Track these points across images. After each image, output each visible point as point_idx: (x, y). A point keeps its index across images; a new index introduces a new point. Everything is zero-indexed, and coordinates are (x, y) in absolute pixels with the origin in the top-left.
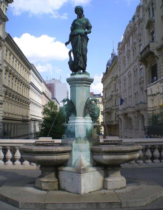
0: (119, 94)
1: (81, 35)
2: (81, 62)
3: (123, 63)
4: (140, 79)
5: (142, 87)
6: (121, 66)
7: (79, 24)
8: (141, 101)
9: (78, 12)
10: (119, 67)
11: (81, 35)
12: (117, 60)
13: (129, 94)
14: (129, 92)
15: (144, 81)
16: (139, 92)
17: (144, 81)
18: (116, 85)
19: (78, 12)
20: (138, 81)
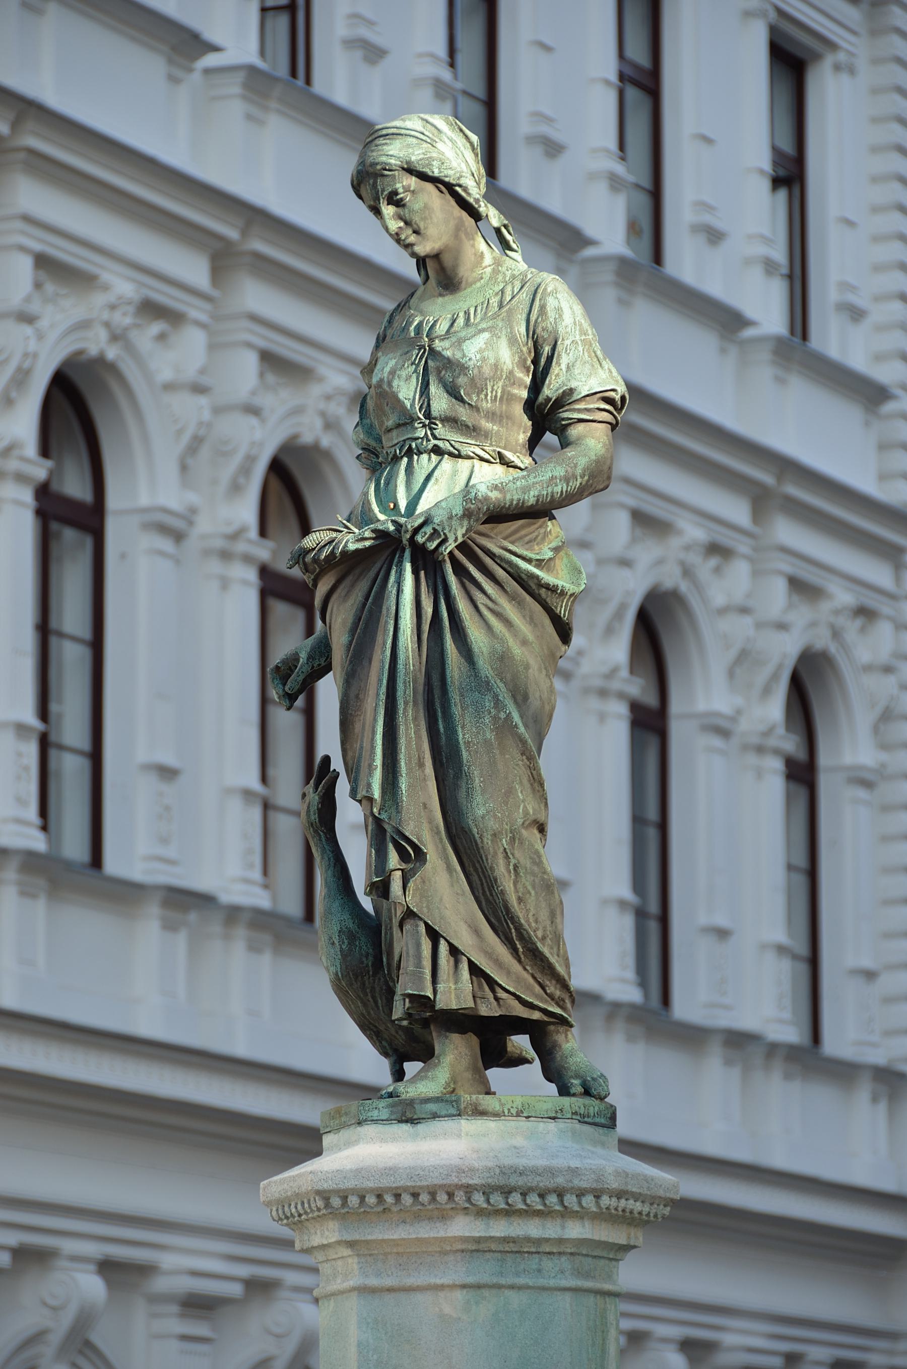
1: (427, 562)
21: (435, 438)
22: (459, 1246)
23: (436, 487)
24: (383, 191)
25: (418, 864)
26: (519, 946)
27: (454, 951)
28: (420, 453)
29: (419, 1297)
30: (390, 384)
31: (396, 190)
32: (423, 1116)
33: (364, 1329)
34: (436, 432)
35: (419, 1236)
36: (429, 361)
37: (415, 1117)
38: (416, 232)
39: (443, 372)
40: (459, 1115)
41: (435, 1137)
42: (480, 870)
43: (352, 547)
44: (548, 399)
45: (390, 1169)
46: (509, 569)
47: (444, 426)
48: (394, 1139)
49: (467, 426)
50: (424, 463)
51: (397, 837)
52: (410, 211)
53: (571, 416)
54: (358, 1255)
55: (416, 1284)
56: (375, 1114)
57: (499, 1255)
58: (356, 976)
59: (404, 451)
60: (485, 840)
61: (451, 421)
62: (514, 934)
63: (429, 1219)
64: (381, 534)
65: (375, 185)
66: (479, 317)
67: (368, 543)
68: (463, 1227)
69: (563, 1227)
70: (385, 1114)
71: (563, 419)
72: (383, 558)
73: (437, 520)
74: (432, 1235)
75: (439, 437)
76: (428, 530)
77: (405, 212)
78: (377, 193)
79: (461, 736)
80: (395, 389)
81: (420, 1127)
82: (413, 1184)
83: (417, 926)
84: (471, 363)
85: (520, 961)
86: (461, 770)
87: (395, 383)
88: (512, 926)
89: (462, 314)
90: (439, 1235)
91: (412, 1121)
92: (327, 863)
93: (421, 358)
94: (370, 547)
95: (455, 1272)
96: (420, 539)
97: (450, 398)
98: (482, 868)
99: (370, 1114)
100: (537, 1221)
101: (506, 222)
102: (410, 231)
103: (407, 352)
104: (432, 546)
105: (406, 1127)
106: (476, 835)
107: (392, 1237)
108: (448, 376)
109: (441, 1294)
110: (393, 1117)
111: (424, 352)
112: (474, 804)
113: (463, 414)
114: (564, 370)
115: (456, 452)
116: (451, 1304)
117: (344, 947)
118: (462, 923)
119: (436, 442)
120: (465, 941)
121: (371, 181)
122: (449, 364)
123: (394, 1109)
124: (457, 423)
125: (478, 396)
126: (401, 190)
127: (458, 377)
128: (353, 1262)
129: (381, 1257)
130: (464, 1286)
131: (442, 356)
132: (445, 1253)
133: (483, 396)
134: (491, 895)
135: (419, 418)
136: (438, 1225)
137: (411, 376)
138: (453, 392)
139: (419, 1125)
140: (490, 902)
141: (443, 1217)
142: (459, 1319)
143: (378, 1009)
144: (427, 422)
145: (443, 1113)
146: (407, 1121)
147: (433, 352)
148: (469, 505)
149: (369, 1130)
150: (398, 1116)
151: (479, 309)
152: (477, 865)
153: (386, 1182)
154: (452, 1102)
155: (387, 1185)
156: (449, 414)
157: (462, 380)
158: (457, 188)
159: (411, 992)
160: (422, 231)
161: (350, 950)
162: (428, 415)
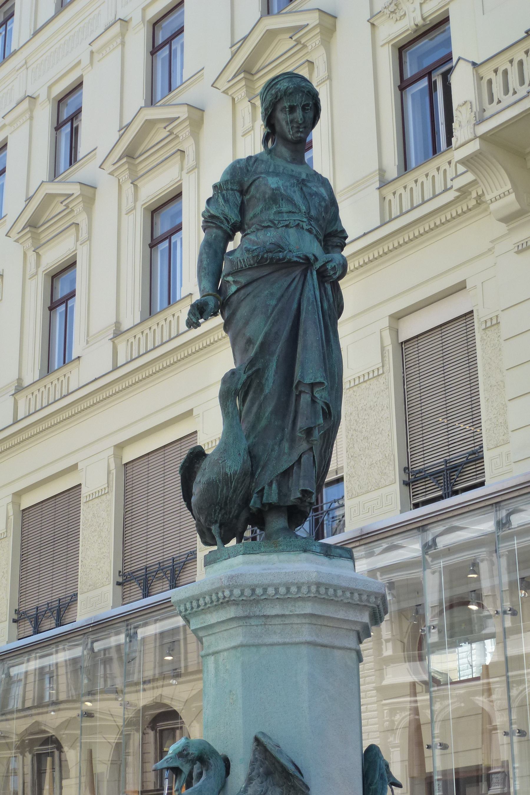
51: (325, 408)
74: (356, 620)
110: (322, 552)
134: (325, 452)
139: (333, 560)
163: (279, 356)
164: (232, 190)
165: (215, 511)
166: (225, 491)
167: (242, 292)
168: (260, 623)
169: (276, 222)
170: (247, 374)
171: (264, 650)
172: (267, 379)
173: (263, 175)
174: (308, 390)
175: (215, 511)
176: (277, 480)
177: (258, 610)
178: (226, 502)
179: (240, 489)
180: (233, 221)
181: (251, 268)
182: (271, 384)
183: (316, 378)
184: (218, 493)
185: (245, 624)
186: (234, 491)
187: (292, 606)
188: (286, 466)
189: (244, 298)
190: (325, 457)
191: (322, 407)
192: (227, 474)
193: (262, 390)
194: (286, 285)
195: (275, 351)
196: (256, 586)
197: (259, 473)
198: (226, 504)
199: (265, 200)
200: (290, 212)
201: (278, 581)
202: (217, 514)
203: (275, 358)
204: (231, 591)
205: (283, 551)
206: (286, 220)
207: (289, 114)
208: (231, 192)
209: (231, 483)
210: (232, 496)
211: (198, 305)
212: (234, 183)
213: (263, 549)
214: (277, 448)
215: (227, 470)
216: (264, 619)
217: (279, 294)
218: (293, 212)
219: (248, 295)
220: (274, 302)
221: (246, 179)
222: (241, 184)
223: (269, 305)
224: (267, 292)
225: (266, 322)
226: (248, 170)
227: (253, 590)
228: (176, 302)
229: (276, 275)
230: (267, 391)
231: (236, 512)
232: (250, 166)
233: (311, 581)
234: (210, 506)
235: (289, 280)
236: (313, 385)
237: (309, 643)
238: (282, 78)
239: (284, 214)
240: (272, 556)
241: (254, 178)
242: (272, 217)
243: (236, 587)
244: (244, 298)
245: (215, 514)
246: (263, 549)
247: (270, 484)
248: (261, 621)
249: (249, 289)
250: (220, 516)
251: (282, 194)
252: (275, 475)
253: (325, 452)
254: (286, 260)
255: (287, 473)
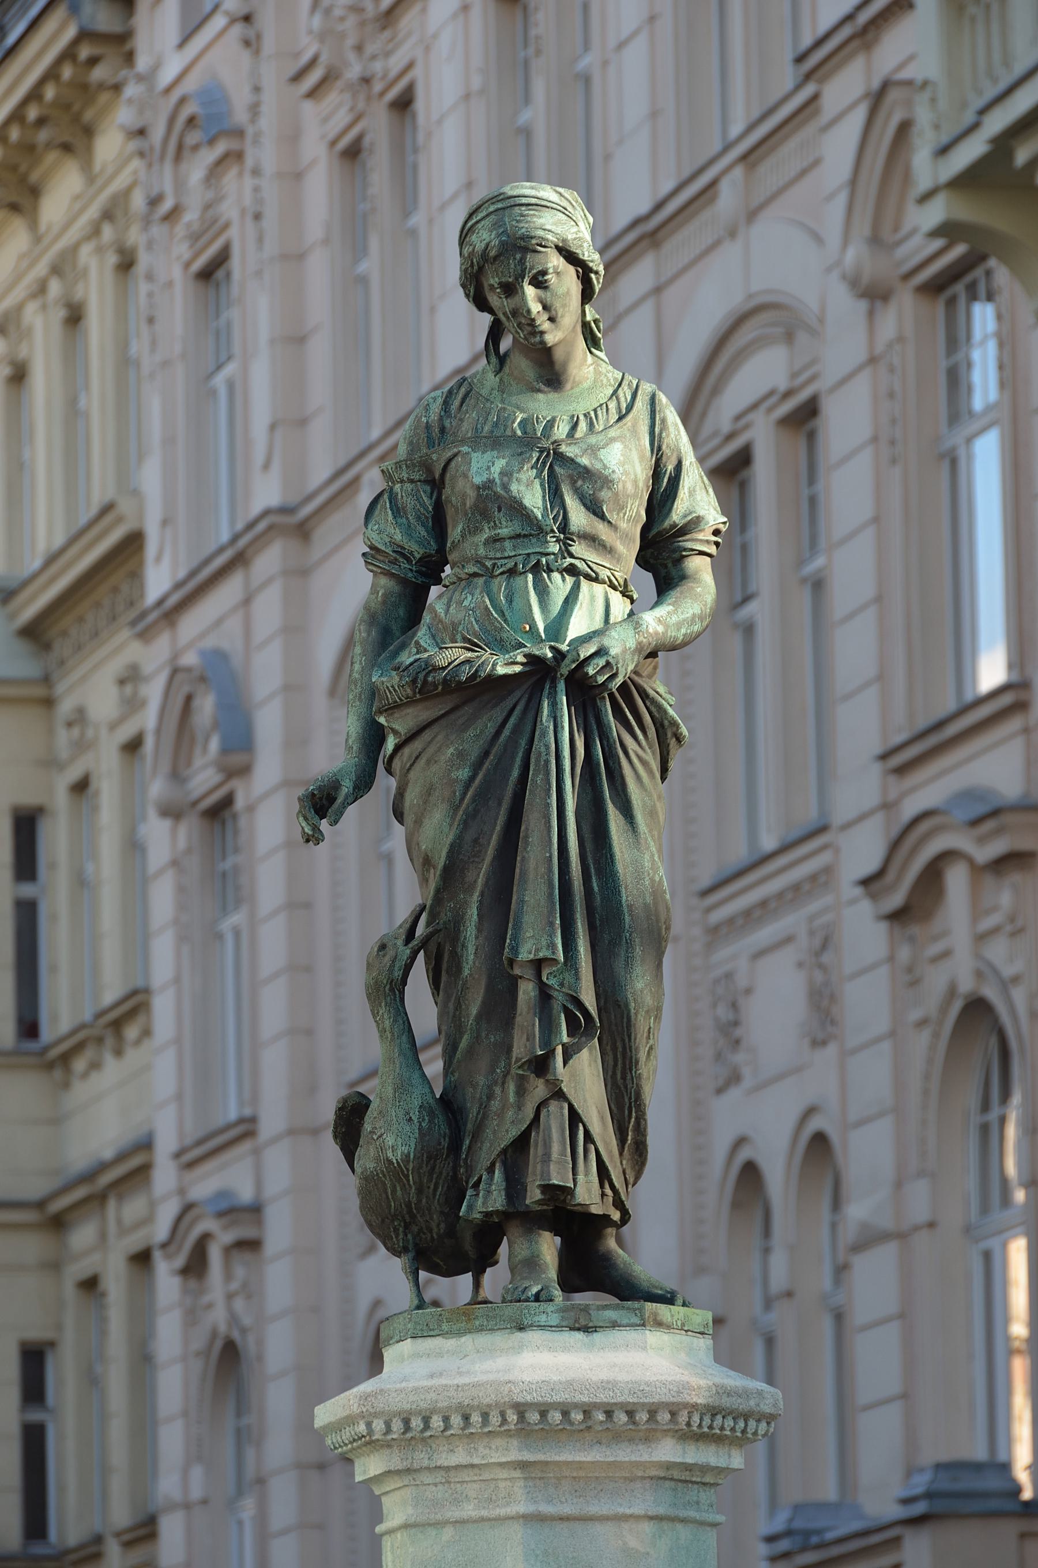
0: (165, 1176)
2: (575, 1118)
3: (315, 149)
4: (903, 760)
5: (977, 1011)
6: (240, 237)
7: (534, 499)
8: (932, 1453)
9: (530, 291)
10: (168, 261)
11: (584, 692)
12: (121, 43)
13: (729, 1116)
14: (731, 1032)
15: (255, 1210)
16: (868, 1155)
17: (255, 1210)
18: (55, 841)
19: (530, 291)
20: (859, 786)
21: (572, 556)
22: (653, 1472)
23: (580, 612)
24: (531, 269)
25: (583, 1039)
26: (629, 1138)
27: (588, 1137)
28: (549, 570)
29: (598, 1528)
30: (506, 487)
31: (547, 269)
32: (601, 1324)
33: (532, 1562)
34: (572, 549)
35: (618, 1459)
36: (557, 468)
37: (591, 1324)
38: (551, 319)
39: (580, 483)
40: (644, 1325)
41: (616, 1348)
42: (620, 1049)
43: (501, 670)
44: (675, 525)
45: (608, 1382)
46: (656, 714)
47: (580, 543)
48: (566, 1349)
49: (604, 547)
50: (560, 585)
51: (571, 1007)
52: (552, 295)
53: (694, 547)
54: (525, 1479)
55: (600, 1513)
56: (543, 1319)
57: (673, 1484)
58: (429, 1158)
59: (530, 565)
60: (639, 1016)
61: (591, 539)
62: (632, 1123)
63: (629, 1440)
64: (533, 660)
65: (522, 261)
66: (601, 422)
67: (518, 669)
68: (668, 1451)
69: (684, 1452)
70: (554, 1319)
71: (685, 550)
72: (525, 687)
73: (613, 652)
74: (633, 1458)
75: (576, 555)
76: (601, 662)
77: (547, 296)
78: (524, 271)
79: (624, 898)
80: (515, 493)
81: (597, 1337)
82: (635, 1400)
83: (562, 1108)
84: (615, 476)
85: (621, 1154)
86: (621, 937)
87: (514, 487)
88: (634, 1114)
89: (582, 417)
90: (642, 1459)
91: (586, 1329)
92: (402, 1027)
93: (544, 463)
94: (520, 673)
95: (642, 1502)
96: (591, 671)
97: (588, 513)
98: (624, 1048)
99: (536, 1319)
100: (713, 1448)
101: (597, 316)
102: (546, 316)
103: (521, 454)
104: (601, 679)
105: (579, 1336)
106: (633, 1011)
107: (584, 1459)
108: (587, 488)
109: (626, 1526)
110: (564, 1324)
111: (547, 456)
112: (634, 975)
113: (601, 529)
114: (687, 494)
115: (594, 575)
116: (637, 1537)
117: (424, 1125)
118: (594, 1108)
119: (573, 561)
120: (596, 1129)
121: (518, 256)
122: (586, 473)
123: (566, 1315)
124: (594, 541)
125: (618, 514)
126: (551, 271)
127: (600, 490)
128: (519, 1489)
129: (553, 1481)
130: (651, 1518)
131: (576, 463)
132: (632, 1479)
133: (622, 515)
134: (624, 1078)
135: (553, 531)
136: (641, 1447)
137: (533, 482)
138: (595, 509)
139: (595, 1334)
140: (618, 1087)
141: (649, 1438)
142: (648, 1554)
143: (434, 1197)
144: (562, 536)
145: (625, 1321)
146: (579, 1329)
147: (559, 456)
148: (641, 638)
149: (533, 1336)
150: (571, 1323)
151: (599, 412)
152: (619, 1044)
153: (603, 1397)
154: (635, 1310)
155: (605, 1400)
156: (588, 530)
157: (604, 494)
158: (593, 276)
159: (556, 1182)
160: (558, 319)
161: (430, 1129)
162: (564, 527)
163: (482, 894)
164: (412, 481)
165: (396, 1230)
166: (399, 1193)
167: (407, 751)
168: (438, 1480)
169: (489, 564)
170: (410, 945)
171: (448, 1533)
172: (463, 946)
173: (465, 449)
174: (529, 973)
175: (396, 1230)
176: (504, 1164)
177: (427, 1456)
178: (410, 1212)
179: (432, 1187)
180: (418, 556)
181: (411, 702)
182: (472, 957)
183: (537, 950)
184: (386, 1193)
185: (412, 1482)
186: (420, 1191)
187: (485, 1447)
188: (514, 1132)
189: (412, 765)
190: (626, 1087)
191: (564, 1006)
192: (390, 1162)
193: (459, 970)
194: (491, 728)
195: (475, 881)
196: (410, 1413)
197: (470, 1147)
198: (413, 1217)
199: (466, 514)
200: (519, 536)
201: (446, 1404)
202: (401, 1236)
203: (476, 896)
204: (369, 1425)
205: (480, 1329)
206: (510, 557)
207: (506, 297)
208: (408, 486)
209: (407, 1176)
210: (419, 1201)
211: (313, 795)
212: (414, 465)
213: (445, 1327)
214: (499, 1093)
215: (390, 1154)
216: (443, 1473)
217: (474, 754)
218: (525, 536)
219: (417, 758)
220: (464, 774)
221: (434, 457)
222: (426, 466)
223: (456, 780)
224: (451, 750)
225: (453, 818)
226: (443, 430)
227: (407, 1422)
228: (821, 321)
229: (468, 709)
230: (466, 972)
231: (443, 1226)
232: (450, 416)
233: (502, 1401)
234: (383, 1221)
235: (499, 714)
236: (538, 964)
237: (524, 1517)
238: (484, 214)
239: (507, 544)
240: (463, 1339)
241: (449, 454)
242: (482, 551)
243: (376, 1415)
244: (412, 765)
245: (397, 1236)
246: (445, 1327)
247: (491, 1170)
248: (440, 1476)
249: (417, 745)
250: (410, 1236)
251: (497, 496)
252: (496, 1152)
253: (624, 1078)
254: (478, 680)
255: (522, 1143)
